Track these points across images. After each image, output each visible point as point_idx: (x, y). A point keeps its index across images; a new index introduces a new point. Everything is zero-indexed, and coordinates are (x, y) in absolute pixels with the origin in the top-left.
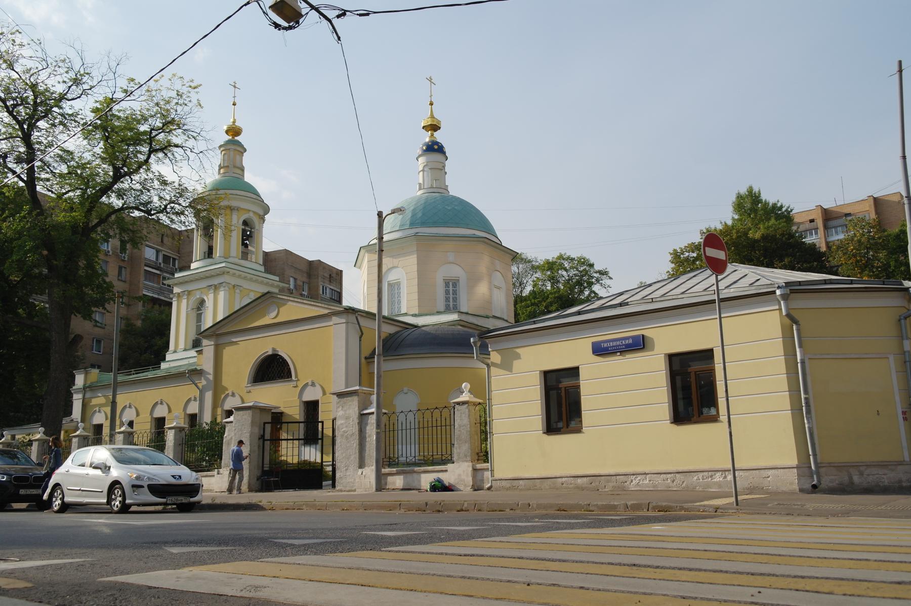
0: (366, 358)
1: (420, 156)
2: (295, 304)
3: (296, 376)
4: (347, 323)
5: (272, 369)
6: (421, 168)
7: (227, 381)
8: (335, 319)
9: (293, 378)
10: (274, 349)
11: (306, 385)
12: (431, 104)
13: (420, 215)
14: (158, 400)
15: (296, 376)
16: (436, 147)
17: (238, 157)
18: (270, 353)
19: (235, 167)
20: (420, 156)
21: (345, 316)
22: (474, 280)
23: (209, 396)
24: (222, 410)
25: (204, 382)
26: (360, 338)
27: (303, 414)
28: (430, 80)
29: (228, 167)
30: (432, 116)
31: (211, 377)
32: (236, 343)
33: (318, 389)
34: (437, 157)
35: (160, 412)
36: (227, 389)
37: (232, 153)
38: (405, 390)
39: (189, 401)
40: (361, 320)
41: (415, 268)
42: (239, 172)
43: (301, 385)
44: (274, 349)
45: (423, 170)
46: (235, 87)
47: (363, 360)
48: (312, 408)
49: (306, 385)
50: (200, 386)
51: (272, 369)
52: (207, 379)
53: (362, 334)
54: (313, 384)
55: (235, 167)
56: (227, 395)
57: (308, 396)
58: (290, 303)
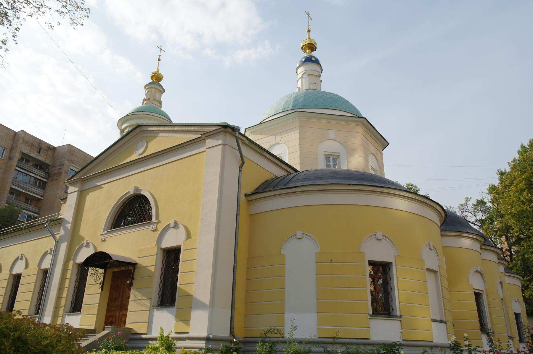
0: (246, 195)
1: (299, 67)
2: (165, 135)
3: (157, 218)
4: (224, 145)
5: (134, 211)
6: (300, 76)
7: (85, 231)
8: (210, 142)
9: (154, 220)
10: (137, 189)
11: (168, 227)
12: (309, 31)
13: (302, 100)
14: (19, 255)
15: (157, 218)
16: (313, 59)
17: (158, 94)
18: (132, 192)
19: (154, 100)
20: (299, 67)
21: (222, 136)
22: (350, 152)
23: (64, 247)
24: (74, 263)
25: (62, 232)
26: (241, 167)
27: (160, 265)
28: (308, 14)
29: (149, 99)
30: (309, 38)
31: (69, 226)
32: (99, 187)
33: (182, 231)
34: (312, 66)
35: (19, 269)
36: (83, 239)
37: (153, 90)
38: (299, 234)
39: (46, 254)
40: (244, 148)
41: (297, 142)
42: (158, 104)
43: (161, 227)
44: (137, 189)
45: (302, 77)
46: (161, 49)
47: (243, 197)
48: (171, 257)
49: (168, 227)
50: (57, 237)
51: (134, 211)
52: (65, 229)
53: (243, 163)
54: (176, 226)
55: (154, 100)
56: (81, 246)
57: (168, 242)
58: (161, 135)
